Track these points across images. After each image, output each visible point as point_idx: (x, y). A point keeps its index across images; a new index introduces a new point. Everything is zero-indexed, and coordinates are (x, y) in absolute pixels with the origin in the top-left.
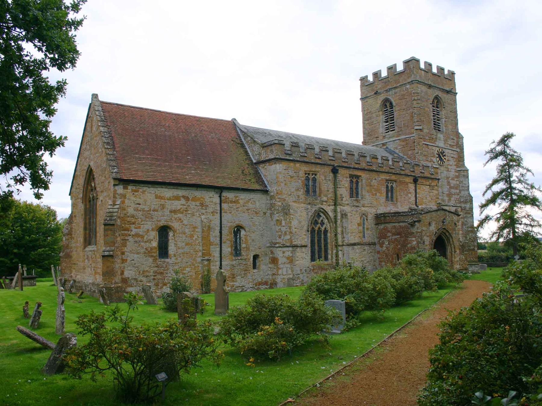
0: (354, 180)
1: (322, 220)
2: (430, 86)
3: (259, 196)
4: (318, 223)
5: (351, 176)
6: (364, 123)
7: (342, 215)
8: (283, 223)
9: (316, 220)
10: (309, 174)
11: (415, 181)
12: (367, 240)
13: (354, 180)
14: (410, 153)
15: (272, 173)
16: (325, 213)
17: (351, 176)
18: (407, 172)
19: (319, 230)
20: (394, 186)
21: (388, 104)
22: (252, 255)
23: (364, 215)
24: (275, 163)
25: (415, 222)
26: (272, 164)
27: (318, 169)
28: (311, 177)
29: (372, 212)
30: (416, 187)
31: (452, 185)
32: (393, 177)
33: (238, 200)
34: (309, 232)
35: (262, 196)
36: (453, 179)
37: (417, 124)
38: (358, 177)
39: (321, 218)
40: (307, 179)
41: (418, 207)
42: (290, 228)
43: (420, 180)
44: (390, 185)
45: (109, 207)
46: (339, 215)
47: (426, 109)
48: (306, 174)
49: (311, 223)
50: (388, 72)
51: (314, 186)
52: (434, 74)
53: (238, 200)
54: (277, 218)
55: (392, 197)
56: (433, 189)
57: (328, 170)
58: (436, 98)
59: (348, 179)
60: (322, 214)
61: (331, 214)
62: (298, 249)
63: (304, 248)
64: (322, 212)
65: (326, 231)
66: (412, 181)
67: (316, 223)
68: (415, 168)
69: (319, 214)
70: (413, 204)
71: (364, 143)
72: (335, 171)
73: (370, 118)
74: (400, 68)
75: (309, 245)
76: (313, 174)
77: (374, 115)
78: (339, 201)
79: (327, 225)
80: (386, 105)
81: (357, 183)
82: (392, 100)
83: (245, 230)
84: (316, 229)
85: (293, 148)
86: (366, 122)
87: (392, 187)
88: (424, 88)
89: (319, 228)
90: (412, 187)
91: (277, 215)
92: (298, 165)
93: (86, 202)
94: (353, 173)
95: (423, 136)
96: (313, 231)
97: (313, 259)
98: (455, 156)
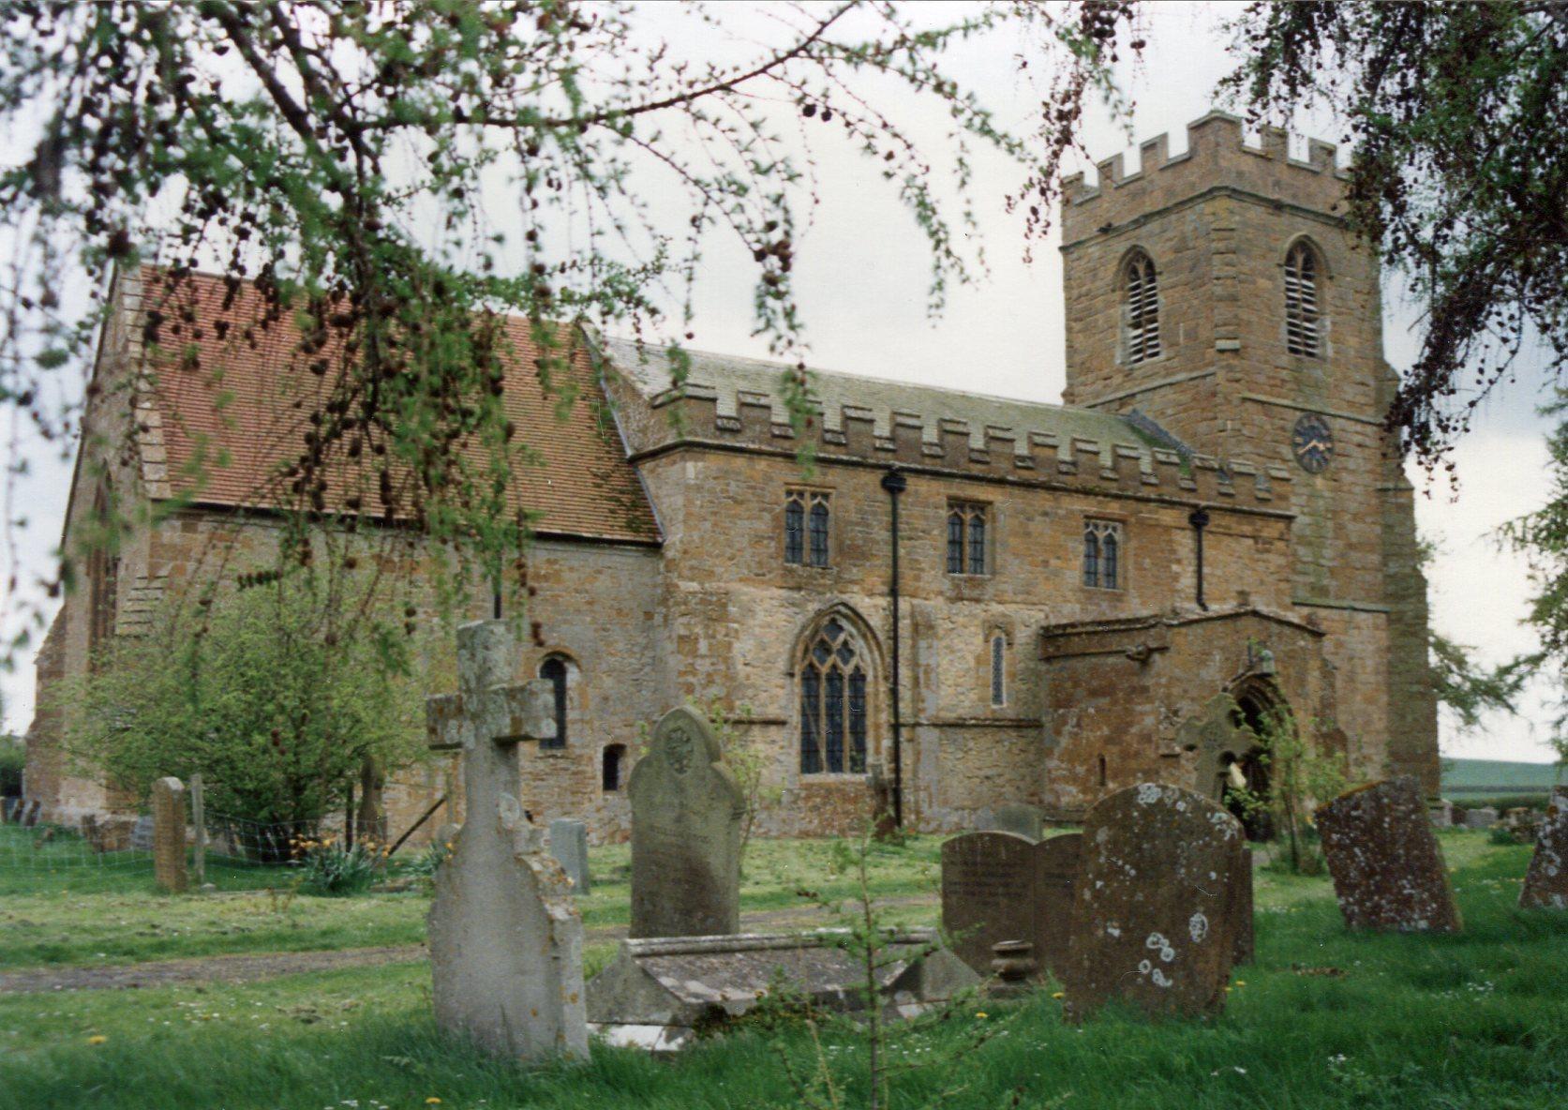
0: (968, 516)
1: (845, 643)
2: (1278, 207)
3: (631, 561)
4: (828, 651)
5: (956, 503)
6: (1069, 330)
7: (916, 626)
8: (703, 646)
9: (822, 642)
10: (801, 494)
11: (1198, 520)
12: (1007, 708)
13: (968, 516)
14: (1203, 427)
15: (675, 489)
16: (856, 617)
17: (956, 503)
18: (1169, 492)
19: (835, 676)
20: (1118, 537)
21: (1141, 268)
22: (604, 744)
23: (999, 633)
24: (683, 459)
25: (1151, 651)
26: (674, 463)
27: (835, 476)
28: (808, 504)
29: (1028, 620)
30: (1199, 541)
31: (1354, 540)
32: (1114, 508)
33: (557, 572)
34: (797, 679)
35: (645, 560)
36: (1355, 517)
37: (1222, 330)
38: (981, 506)
39: (842, 637)
40: (795, 510)
41: (1205, 608)
42: (727, 661)
43: (1215, 521)
44: (1101, 535)
45: (139, 584)
46: (905, 624)
47: (1263, 283)
48: (789, 493)
49: (806, 650)
50: (1144, 160)
51: (820, 533)
52: (1296, 167)
53: (557, 572)
54: (682, 632)
55: (1111, 574)
56: (1268, 551)
57: (872, 479)
58: (1304, 245)
59: (944, 513)
60: (844, 623)
61: (877, 621)
62: (756, 730)
63: (773, 729)
64: (846, 616)
65: (858, 677)
66: (1185, 522)
67: (825, 649)
68: (1199, 477)
69: (833, 621)
70: (1187, 599)
71: (1068, 395)
72: (893, 483)
73: (1090, 312)
74: (1178, 146)
75: (795, 719)
76: (814, 495)
77: (1099, 303)
78: (906, 582)
79: (867, 659)
80: (1135, 271)
81: (979, 523)
82: (1153, 255)
83: (579, 667)
84: (824, 670)
85: (746, 410)
86: (1077, 326)
87: (1110, 541)
88: (1257, 214)
89: (834, 667)
90: (1185, 541)
91: (682, 620)
92: (762, 464)
93: (97, 571)
94: (961, 494)
95: (1247, 373)
96: (810, 676)
97: (809, 761)
98: (1368, 442)
